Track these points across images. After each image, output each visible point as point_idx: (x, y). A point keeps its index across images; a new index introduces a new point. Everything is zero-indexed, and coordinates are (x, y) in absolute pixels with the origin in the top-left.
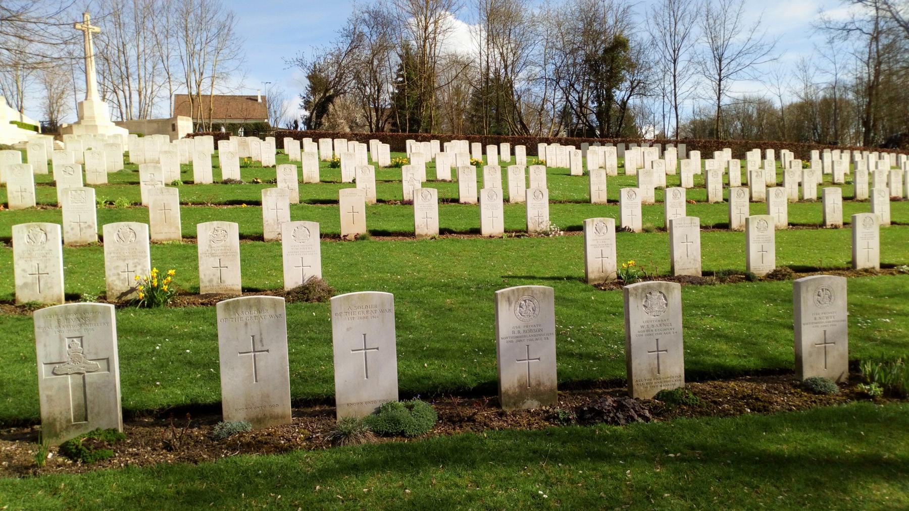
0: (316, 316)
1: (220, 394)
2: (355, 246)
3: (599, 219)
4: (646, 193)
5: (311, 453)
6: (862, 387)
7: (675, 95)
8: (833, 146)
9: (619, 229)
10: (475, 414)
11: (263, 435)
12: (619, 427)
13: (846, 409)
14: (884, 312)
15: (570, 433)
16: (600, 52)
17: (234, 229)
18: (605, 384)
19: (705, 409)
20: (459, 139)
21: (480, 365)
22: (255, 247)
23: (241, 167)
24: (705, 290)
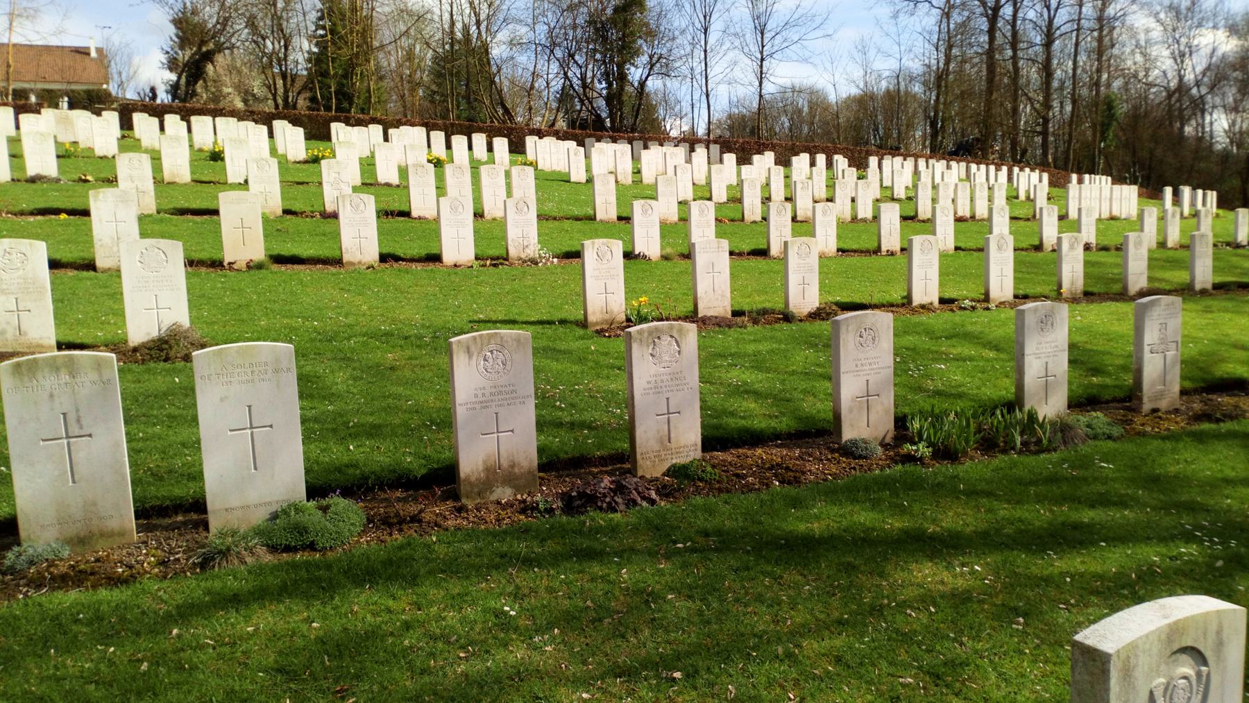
0: (180, 383)
1: (14, 505)
2: (246, 277)
3: (601, 240)
4: (666, 208)
5: (165, 584)
6: (908, 448)
7: (706, 77)
8: (895, 151)
9: (628, 255)
10: (421, 511)
11: (87, 562)
12: (616, 515)
13: (889, 476)
14: (939, 357)
15: (552, 528)
16: (609, 11)
17: (37, 253)
18: (603, 461)
19: (724, 485)
20: (413, 125)
21: (432, 443)
22: (81, 280)
23: (58, 157)
24: (734, 333)
